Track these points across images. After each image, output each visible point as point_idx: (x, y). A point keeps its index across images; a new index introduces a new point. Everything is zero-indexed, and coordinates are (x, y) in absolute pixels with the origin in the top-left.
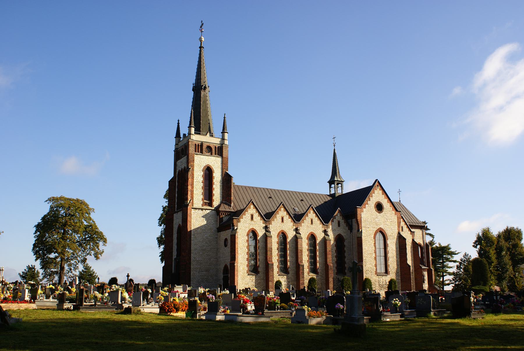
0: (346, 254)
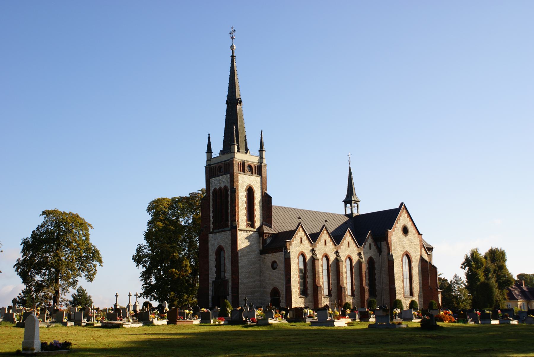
0: (376, 277)
